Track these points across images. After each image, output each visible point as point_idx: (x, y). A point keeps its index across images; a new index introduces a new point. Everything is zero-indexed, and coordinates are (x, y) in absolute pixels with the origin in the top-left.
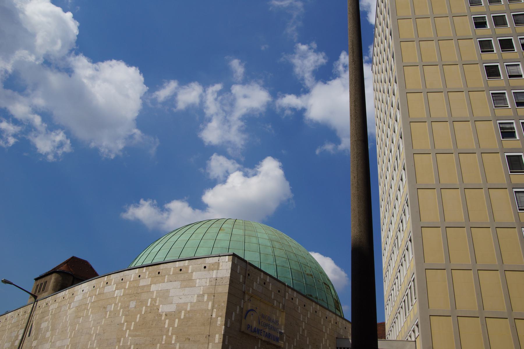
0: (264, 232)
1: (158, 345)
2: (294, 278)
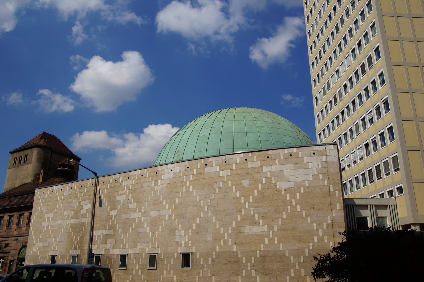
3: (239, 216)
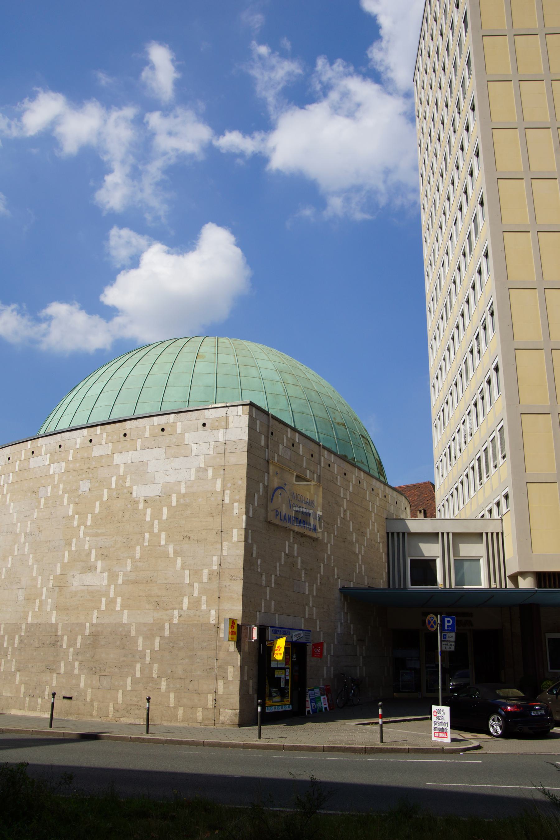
0: (266, 358)
1: (138, 548)
2: (319, 431)
3: (67, 553)
